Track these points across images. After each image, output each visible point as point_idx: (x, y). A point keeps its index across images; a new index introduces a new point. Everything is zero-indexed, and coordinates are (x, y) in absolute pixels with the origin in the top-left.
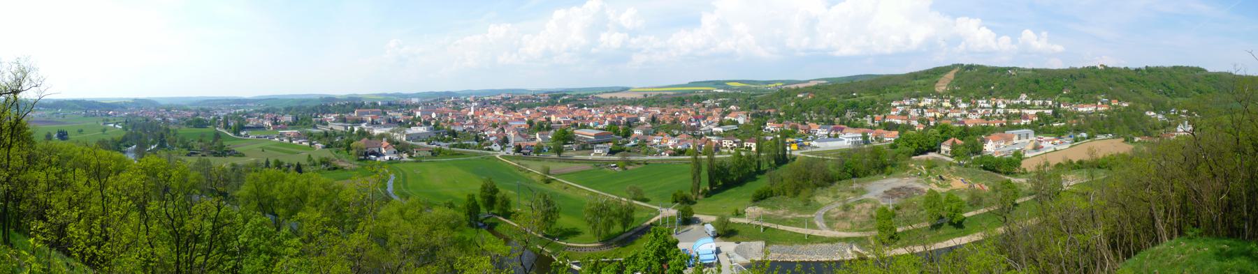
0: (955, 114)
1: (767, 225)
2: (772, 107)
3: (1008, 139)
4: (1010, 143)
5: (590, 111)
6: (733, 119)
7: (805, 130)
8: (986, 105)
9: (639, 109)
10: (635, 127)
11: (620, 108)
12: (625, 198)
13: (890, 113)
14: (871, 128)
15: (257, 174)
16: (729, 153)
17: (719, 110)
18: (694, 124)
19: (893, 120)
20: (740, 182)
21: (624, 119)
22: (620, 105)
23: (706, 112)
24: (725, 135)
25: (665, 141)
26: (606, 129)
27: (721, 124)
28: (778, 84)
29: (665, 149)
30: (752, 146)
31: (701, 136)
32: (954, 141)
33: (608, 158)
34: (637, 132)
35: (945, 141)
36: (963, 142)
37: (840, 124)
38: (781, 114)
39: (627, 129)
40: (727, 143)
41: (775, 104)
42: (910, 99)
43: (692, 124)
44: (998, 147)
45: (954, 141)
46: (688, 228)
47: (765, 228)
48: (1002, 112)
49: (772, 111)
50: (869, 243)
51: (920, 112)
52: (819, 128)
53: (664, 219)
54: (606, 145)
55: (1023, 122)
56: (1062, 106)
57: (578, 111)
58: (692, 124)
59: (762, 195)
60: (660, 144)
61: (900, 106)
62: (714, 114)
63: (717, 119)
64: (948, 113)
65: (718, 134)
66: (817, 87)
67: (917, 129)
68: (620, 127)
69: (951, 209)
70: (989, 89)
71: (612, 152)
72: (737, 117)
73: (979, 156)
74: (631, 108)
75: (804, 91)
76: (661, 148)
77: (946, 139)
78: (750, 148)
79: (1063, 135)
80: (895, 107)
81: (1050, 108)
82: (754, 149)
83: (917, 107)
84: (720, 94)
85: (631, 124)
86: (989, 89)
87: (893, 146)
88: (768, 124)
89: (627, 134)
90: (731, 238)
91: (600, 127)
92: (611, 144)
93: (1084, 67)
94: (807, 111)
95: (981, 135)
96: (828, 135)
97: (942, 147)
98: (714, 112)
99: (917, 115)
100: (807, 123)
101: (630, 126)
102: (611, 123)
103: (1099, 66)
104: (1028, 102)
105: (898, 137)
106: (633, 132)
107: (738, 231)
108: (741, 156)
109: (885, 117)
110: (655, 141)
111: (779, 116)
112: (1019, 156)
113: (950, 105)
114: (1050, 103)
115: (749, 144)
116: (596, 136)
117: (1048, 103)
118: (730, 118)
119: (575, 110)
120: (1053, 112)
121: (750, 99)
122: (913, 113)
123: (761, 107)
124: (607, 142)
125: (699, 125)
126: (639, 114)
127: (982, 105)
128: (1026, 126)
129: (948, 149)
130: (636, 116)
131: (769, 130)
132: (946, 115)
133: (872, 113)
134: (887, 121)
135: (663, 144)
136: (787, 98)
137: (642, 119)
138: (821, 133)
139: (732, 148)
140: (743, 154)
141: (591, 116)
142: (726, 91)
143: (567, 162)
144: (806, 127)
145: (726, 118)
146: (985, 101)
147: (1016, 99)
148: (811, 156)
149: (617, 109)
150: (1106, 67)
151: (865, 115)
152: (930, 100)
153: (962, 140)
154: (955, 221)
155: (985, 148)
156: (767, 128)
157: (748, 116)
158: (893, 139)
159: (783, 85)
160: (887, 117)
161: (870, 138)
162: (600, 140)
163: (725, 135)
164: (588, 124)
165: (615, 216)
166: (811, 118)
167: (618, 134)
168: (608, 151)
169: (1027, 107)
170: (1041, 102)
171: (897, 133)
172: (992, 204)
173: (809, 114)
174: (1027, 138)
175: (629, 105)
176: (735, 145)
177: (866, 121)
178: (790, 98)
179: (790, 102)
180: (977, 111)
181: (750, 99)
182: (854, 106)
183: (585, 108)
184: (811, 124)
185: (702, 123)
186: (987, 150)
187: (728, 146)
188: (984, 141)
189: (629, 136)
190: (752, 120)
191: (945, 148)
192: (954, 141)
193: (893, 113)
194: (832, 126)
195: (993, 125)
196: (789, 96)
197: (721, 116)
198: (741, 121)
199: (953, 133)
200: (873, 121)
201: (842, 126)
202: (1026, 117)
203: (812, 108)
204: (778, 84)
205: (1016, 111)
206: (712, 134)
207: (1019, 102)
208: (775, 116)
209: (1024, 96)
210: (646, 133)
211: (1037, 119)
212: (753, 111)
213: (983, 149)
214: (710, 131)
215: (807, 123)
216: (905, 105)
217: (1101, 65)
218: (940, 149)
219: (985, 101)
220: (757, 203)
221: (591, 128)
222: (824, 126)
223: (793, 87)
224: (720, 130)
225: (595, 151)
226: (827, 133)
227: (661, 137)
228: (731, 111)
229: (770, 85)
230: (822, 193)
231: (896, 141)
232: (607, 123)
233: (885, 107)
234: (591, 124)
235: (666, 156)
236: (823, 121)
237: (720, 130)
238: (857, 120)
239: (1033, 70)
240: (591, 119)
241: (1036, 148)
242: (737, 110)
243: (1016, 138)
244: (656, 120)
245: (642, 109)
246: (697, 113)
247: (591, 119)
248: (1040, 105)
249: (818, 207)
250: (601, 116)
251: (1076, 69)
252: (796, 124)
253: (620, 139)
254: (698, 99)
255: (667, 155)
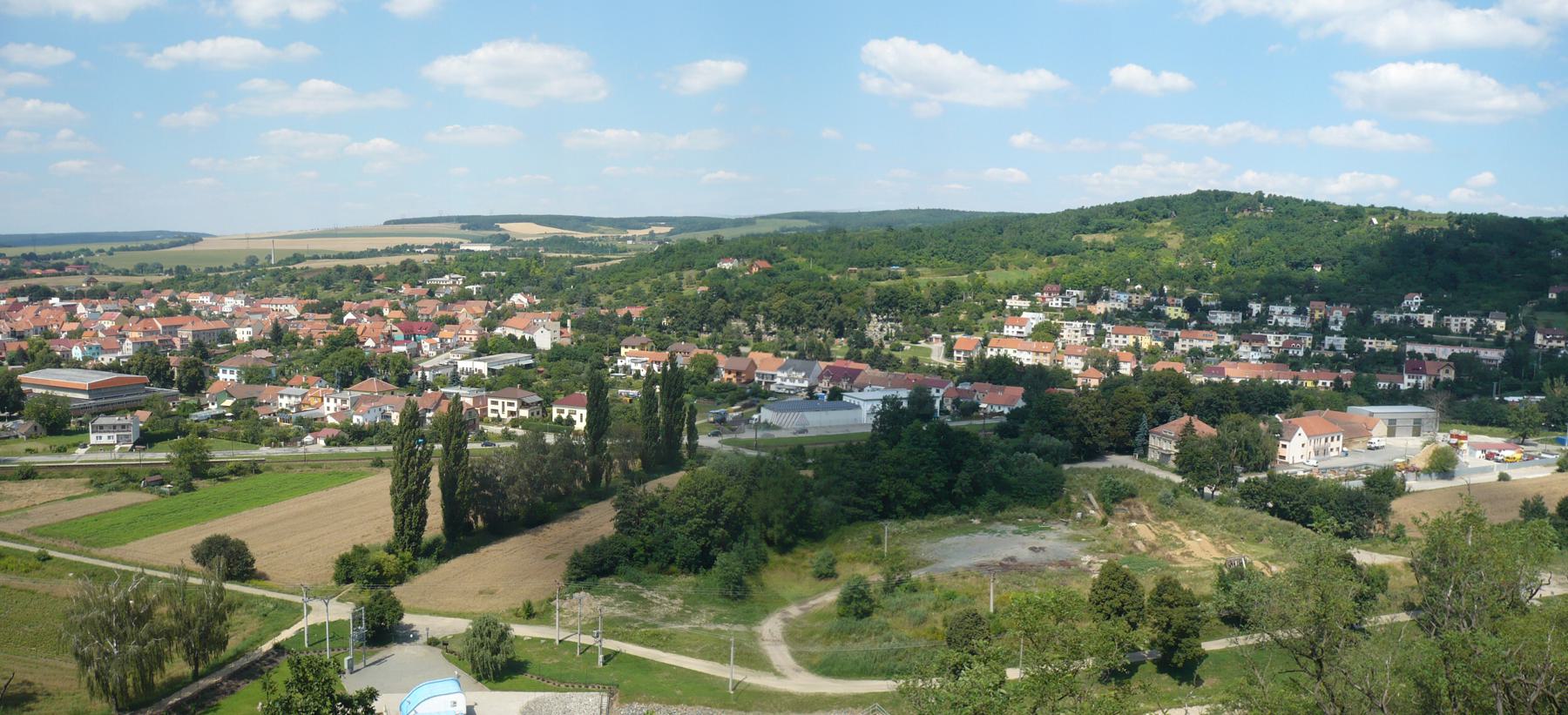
0: (1196, 343)
1: (612, 645)
3: (1353, 434)
4: (1359, 446)
5: (73, 308)
6: (519, 335)
7: (738, 373)
8: (1292, 322)
9: (229, 304)
10: (220, 359)
11: (173, 299)
12: (198, 576)
13: (1001, 330)
14: (940, 371)
16: (507, 436)
17: (479, 306)
18: (403, 349)
19: (1011, 353)
20: (533, 520)
21: (186, 333)
22: (170, 292)
23: (439, 313)
24: (495, 383)
25: (314, 402)
26: (127, 369)
27: (482, 350)
28: (657, 230)
29: (312, 425)
30: (576, 418)
31: (425, 385)
32: (1189, 426)
33: (134, 457)
34: (227, 375)
35: (1162, 423)
36: (1213, 431)
37: (849, 357)
39: (196, 364)
40: (501, 407)
42: (1062, 292)
43: (396, 349)
44: (1321, 452)
45: (1189, 426)
46: (383, 652)
47: (609, 657)
48: (1341, 343)
49: (636, 312)
50: (513, 427)
51: (1091, 332)
52: (783, 368)
53: (315, 629)
54: (127, 419)
55: (1406, 383)
56: (1539, 339)
57: (30, 310)
58: (396, 349)
59: (602, 563)
60: (299, 410)
61: (1033, 309)
62: (461, 319)
63: (472, 334)
64: (1177, 339)
65: (474, 381)
67: (1080, 382)
68: (173, 360)
69: (1169, 625)
71: (146, 439)
72: (531, 327)
73: (1263, 476)
74: (205, 299)
75: (741, 250)
76: (300, 421)
77: (1163, 418)
78: (571, 422)
79: (1536, 434)
80: (1017, 313)
81: (1499, 343)
82: (580, 425)
83: (1083, 317)
84: (486, 257)
85: (203, 357)
87: (1006, 431)
88: (623, 350)
89: (196, 383)
90: (508, 682)
91: (106, 359)
92: (143, 415)
95: (1273, 412)
96: (810, 390)
97: (1153, 442)
98: (463, 312)
99: (1081, 339)
100: (743, 349)
101: (205, 356)
102: (143, 348)
104: (1428, 320)
105: (1021, 404)
106: (214, 373)
107: (526, 663)
108: (545, 448)
109: (985, 343)
110: (284, 402)
112: (1385, 485)
113: (1186, 316)
114: (1501, 325)
115: (567, 411)
116: (94, 390)
117: (1491, 328)
118: (509, 331)
119: (17, 307)
120: (1506, 359)
121: (571, 273)
122: (1072, 333)
124: (133, 409)
125: (416, 353)
126: (233, 317)
127: (1282, 321)
128: (1414, 397)
129: (1170, 447)
130: (222, 324)
131: (626, 369)
132: (1169, 344)
133: (950, 328)
134: (990, 353)
135: (307, 413)
136: (686, 274)
137: (243, 334)
138: (788, 383)
139: (515, 424)
140: (550, 439)
141: (74, 326)
142: (497, 248)
144: (739, 363)
145: (498, 331)
146: (1291, 310)
147: (1391, 310)
148: (754, 453)
149: (161, 304)
152: (1123, 297)
153: (1213, 423)
154: (1178, 659)
155: (1281, 451)
156: (620, 363)
157: (564, 325)
158: (1006, 411)
159: (670, 233)
160: (993, 342)
161: (937, 405)
162: (107, 401)
163: (495, 383)
164: (67, 354)
165: (169, 635)
167: (168, 382)
168: (133, 435)
169: (1425, 336)
170: (1469, 322)
171: (1020, 390)
172: (1285, 621)
174: (1417, 433)
175: (200, 290)
176: (524, 413)
177: (928, 352)
178: (693, 273)
180: (1263, 340)
181: (571, 273)
182: (889, 304)
183: (55, 301)
184: (757, 356)
185: (426, 346)
186: (1289, 460)
187: (504, 416)
188: (1279, 433)
189: (203, 387)
190: (574, 337)
191: (1163, 442)
192: (1189, 427)
193: (1009, 330)
194: (823, 365)
195: (1310, 384)
197: (483, 324)
198: (544, 340)
199: (1188, 403)
200: (949, 354)
201: (853, 365)
202: (1418, 365)
204: (657, 230)
205: (1388, 345)
206: (455, 380)
207: (1398, 317)
209: (1415, 300)
210: (254, 376)
211: (1452, 375)
212: (579, 311)
213: (1276, 451)
214: (450, 371)
215: (743, 349)
216: (1046, 308)
218: (1145, 447)
219: (1291, 310)
220: (588, 582)
221: (77, 365)
222: (799, 363)
223: (703, 237)
224: (481, 366)
225: (93, 438)
226: (806, 384)
227: (302, 391)
228: (515, 310)
229: (631, 233)
230: (784, 563)
231: (1015, 415)
232: (128, 349)
233: (992, 308)
234: (77, 353)
235: (317, 445)
236: (793, 348)
237: (481, 366)
238: (901, 348)
239: (1450, 216)
240: (76, 335)
241: (1443, 466)
242: (533, 307)
243: (1380, 428)
244: (286, 336)
245: (240, 303)
246: (412, 316)
247: (76, 335)
248: (1464, 333)
249: (773, 603)
250: (108, 325)
252: (710, 352)
253: (174, 397)
254: (411, 272)
255: (322, 442)
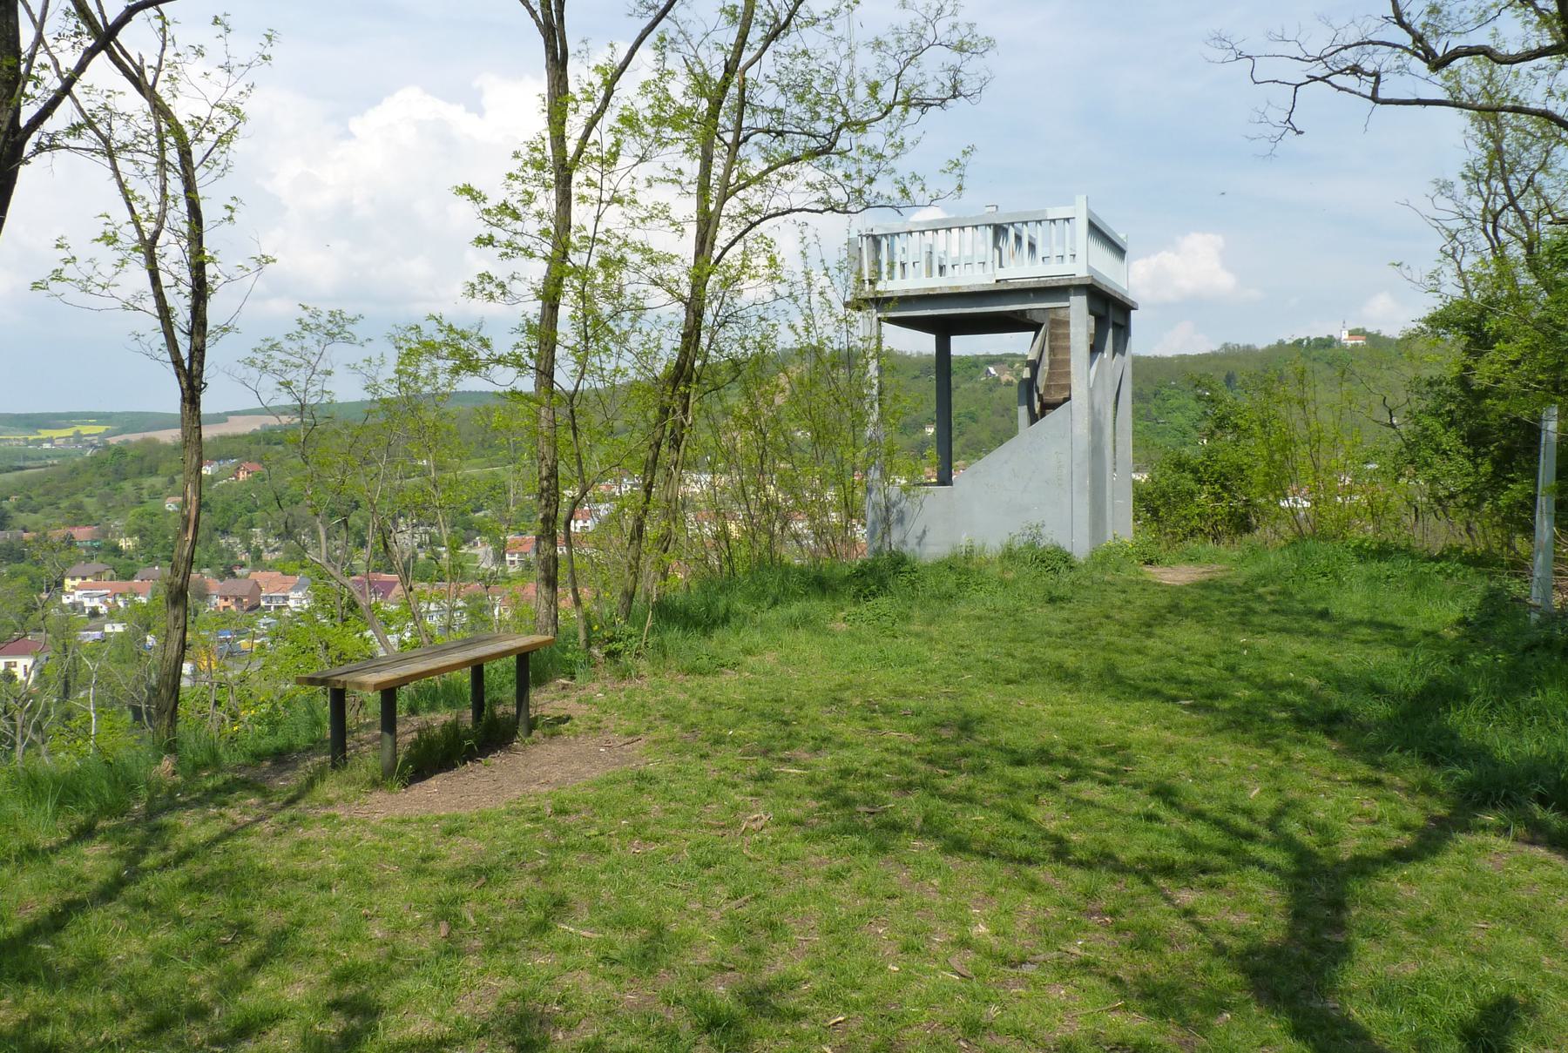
2: (79, 516)
7: (238, 600)
15: (662, 787)
38: (125, 543)
41: (90, 504)
49: (82, 534)
66: (267, 438)
70: (918, 436)
86: (918, 436)
88: (68, 582)
93: (1281, 344)
94: (236, 528)
103: (1345, 335)
111: (116, 551)
123: (24, 518)
136: (148, 482)
143: (1086, 467)
150: (1375, 340)
151: (467, 531)
166: (257, 556)
173: (246, 539)
178: (158, 481)
179: (156, 494)
184: (259, 576)
196: (153, 472)
200: (499, 558)
203: (258, 515)
204: (85, 430)
208: (95, 551)
217: (1352, 333)
229: (45, 434)
251: (1248, 353)
